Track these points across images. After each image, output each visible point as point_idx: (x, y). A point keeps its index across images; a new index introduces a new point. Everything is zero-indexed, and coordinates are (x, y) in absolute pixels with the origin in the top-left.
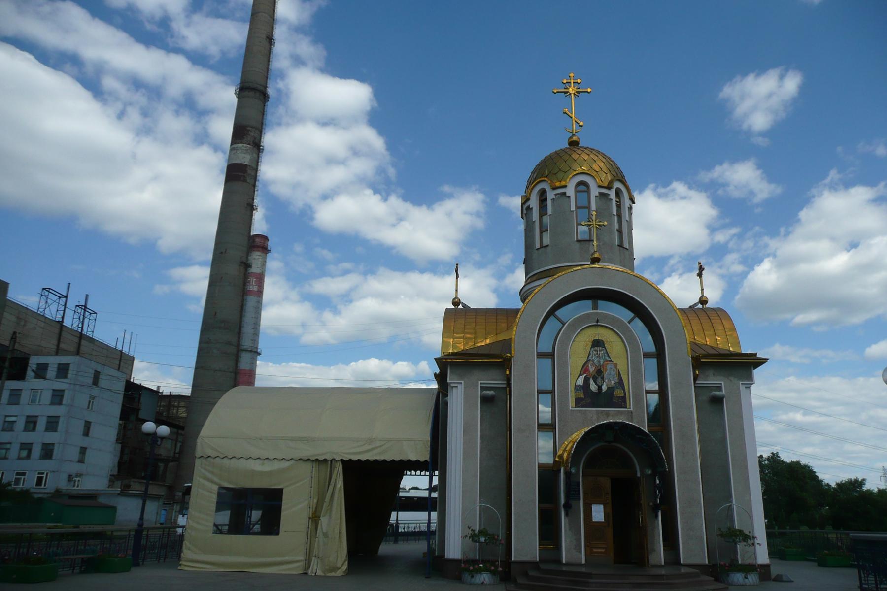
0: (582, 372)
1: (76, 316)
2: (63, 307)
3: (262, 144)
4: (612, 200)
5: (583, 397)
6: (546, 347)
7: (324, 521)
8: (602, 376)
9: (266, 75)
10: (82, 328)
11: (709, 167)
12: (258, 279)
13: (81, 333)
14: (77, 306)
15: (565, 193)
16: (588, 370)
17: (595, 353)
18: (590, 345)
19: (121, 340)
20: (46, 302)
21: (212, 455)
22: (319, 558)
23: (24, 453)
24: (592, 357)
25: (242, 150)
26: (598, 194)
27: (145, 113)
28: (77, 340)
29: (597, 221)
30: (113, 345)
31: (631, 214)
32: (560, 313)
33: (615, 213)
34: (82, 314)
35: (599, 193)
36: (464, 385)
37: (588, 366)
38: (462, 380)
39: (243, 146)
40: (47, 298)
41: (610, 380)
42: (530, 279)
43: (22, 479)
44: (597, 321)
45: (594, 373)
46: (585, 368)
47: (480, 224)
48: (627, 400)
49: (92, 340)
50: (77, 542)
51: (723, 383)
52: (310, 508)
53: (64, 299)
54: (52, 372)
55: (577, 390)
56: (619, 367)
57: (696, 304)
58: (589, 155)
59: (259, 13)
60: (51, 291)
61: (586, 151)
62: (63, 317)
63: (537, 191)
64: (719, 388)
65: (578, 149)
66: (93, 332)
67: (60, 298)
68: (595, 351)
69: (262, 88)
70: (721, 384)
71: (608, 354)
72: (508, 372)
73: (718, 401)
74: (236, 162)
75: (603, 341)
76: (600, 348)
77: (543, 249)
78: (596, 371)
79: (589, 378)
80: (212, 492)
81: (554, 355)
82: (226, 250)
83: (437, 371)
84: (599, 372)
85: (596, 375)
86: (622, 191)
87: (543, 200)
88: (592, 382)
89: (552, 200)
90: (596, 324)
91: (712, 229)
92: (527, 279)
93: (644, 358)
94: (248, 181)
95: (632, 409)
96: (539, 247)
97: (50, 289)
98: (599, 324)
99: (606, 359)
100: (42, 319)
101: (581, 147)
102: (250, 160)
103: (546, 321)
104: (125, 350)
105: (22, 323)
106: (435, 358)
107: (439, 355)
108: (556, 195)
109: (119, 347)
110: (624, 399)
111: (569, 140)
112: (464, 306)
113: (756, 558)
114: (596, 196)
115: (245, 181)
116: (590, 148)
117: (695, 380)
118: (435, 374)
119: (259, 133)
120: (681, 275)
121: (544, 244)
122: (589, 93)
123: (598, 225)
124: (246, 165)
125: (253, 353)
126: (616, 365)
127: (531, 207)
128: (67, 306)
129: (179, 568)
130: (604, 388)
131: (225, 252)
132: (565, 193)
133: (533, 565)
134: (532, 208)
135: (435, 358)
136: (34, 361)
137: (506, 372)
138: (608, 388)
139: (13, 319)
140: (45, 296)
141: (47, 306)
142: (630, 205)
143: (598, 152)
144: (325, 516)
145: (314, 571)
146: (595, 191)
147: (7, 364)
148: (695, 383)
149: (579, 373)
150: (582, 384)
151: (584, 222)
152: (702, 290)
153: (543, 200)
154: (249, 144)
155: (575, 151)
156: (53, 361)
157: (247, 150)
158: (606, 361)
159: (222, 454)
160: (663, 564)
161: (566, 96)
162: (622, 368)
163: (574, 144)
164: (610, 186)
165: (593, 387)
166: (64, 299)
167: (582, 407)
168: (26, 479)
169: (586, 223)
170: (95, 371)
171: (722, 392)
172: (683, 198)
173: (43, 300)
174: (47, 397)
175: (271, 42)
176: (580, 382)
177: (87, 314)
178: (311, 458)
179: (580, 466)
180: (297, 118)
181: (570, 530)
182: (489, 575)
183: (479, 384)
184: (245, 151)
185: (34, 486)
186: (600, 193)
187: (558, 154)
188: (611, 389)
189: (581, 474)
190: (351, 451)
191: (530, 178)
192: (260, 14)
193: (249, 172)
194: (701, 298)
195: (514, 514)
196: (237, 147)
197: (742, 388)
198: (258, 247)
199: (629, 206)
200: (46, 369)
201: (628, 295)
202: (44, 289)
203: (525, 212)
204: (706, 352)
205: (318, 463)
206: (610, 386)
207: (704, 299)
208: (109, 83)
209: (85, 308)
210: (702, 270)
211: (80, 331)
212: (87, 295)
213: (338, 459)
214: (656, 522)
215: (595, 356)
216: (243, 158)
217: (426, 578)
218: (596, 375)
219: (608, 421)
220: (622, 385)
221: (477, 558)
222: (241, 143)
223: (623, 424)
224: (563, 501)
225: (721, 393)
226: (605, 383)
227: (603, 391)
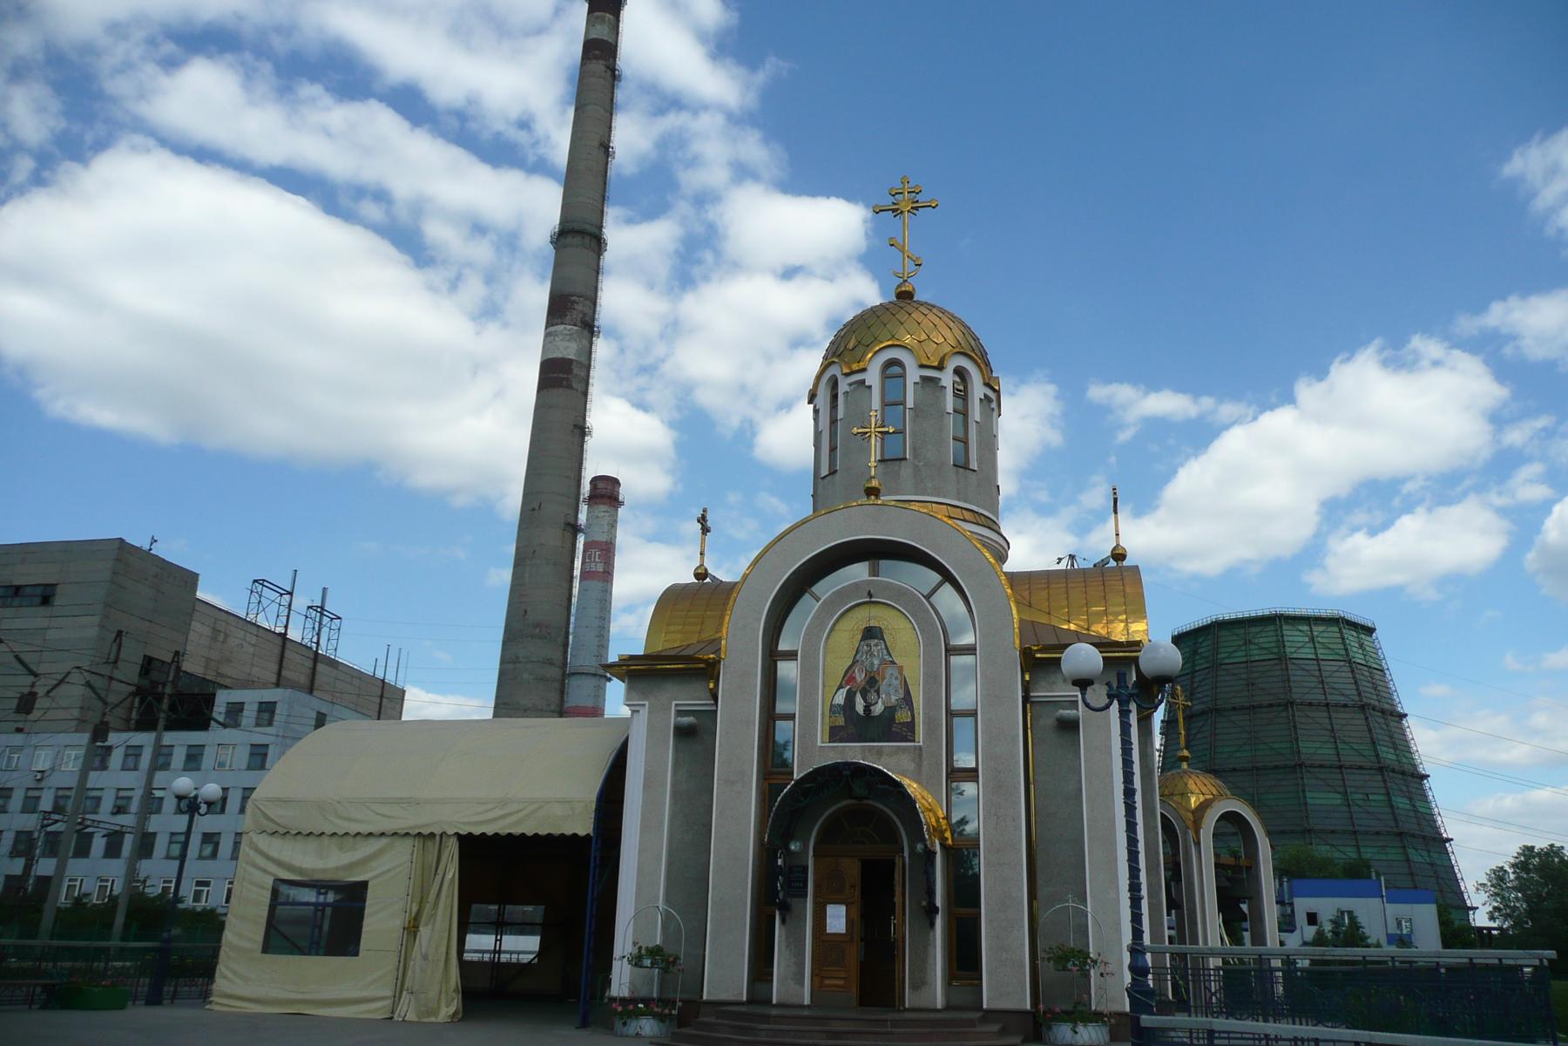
0: (843, 682)
1: (309, 624)
2: (287, 610)
3: (596, 323)
4: (945, 388)
5: (843, 724)
7: (424, 932)
8: (876, 688)
9: (601, 208)
10: (318, 643)
11: (1480, 307)
12: (604, 552)
13: (316, 653)
14: (309, 607)
15: (863, 382)
16: (855, 678)
19: (381, 663)
20: (260, 602)
21: (314, 832)
22: (412, 993)
23: (208, 850)
24: (862, 656)
25: (562, 335)
26: (918, 380)
27: (490, 279)
28: (309, 664)
30: (368, 669)
34: (318, 619)
35: (921, 377)
36: (649, 708)
37: (854, 672)
39: (565, 328)
40: (260, 596)
41: (888, 695)
43: (205, 892)
46: (848, 675)
47: (1055, 438)
49: (333, 664)
50: (136, 980)
52: (406, 912)
53: (288, 596)
54: (249, 714)
56: (906, 673)
59: (586, 105)
60: (265, 583)
61: (921, 308)
62: (286, 627)
66: (336, 649)
67: (281, 595)
69: (594, 230)
71: (888, 651)
72: (711, 686)
74: (554, 356)
76: (876, 641)
78: (868, 678)
80: (263, 888)
82: (541, 504)
86: (967, 370)
90: (868, 599)
91: (1498, 419)
94: (574, 386)
95: (921, 744)
97: (264, 580)
98: (873, 599)
99: (884, 659)
100: (254, 630)
102: (577, 351)
104: (390, 679)
105: (221, 638)
108: (850, 385)
109: (380, 675)
110: (911, 726)
111: (897, 289)
114: (915, 383)
115: (570, 387)
116: (929, 305)
119: (592, 306)
120: (1430, 510)
122: (934, 207)
124: (571, 361)
125: (598, 678)
126: (901, 669)
128: (292, 608)
129: (208, 1007)
131: (540, 507)
132: (863, 382)
136: (223, 698)
137: (708, 686)
139: (207, 631)
140: (257, 592)
141: (261, 609)
143: (943, 312)
144: (426, 925)
145: (403, 1014)
146: (913, 375)
147: (165, 706)
154: (575, 325)
155: (902, 308)
156: (251, 698)
157: (571, 335)
158: (883, 662)
159: (283, 827)
161: (895, 216)
163: (905, 296)
165: (860, 706)
166: (287, 597)
167: (841, 742)
168: (210, 892)
169: (860, 430)
170: (318, 712)
171: (1078, 710)
172: (1436, 364)
173: (255, 598)
174: (242, 756)
175: (608, 151)
176: (840, 699)
177: (326, 620)
178: (411, 832)
179: (809, 839)
180: (736, 267)
181: (787, 947)
182: (652, 1021)
183: (673, 705)
184: (568, 337)
185: (224, 904)
186: (925, 379)
187: (874, 312)
188: (890, 711)
189: (811, 853)
190: (466, 820)
192: (589, 107)
193: (576, 371)
195: (711, 921)
196: (555, 331)
198: (603, 496)
200: (242, 710)
201: (918, 548)
202: (255, 581)
205: (422, 840)
206: (889, 705)
208: (437, 231)
209: (321, 609)
211: (315, 649)
212: (325, 589)
213: (450, 832)
214: (931, 934)
216: (566, 348)
217: (576, 1028)
220: (909, 703)
221: (655, 995)
222: (562, 323)
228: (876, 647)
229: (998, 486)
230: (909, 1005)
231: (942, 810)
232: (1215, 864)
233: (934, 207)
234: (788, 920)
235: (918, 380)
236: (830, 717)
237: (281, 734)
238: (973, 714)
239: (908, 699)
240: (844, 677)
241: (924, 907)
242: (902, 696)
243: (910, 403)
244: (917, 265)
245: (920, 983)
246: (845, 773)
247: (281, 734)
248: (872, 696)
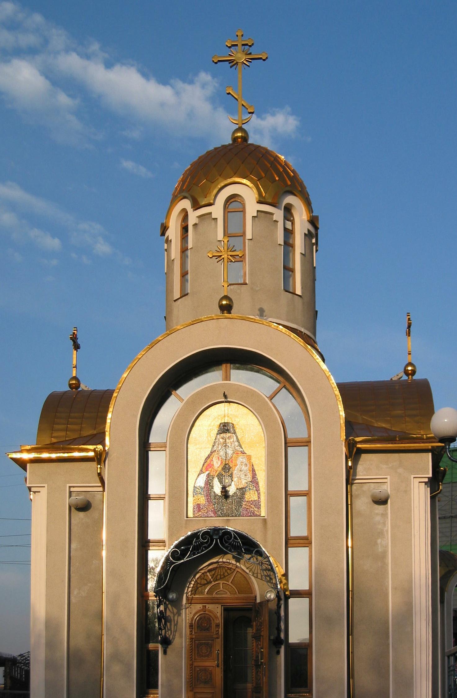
16: (213, 465)
18: (216, 431)
45: (220, 469)
51: (388, 477)
56: (253, 460)
84: (227, 468)
89: (193, 225)
108: (199, 217)
122: (264, 60)
126: (249, 458)
130: (232, 490)
134: (171, 241)
158: (235, 452)
161: (231, 67)
188: (242, 491)
226: (233, 482)
228: (231, 441)
229: (317, 311)
231: (282, 568)
232: (454, 617)
233: (264, 60)
237: (80, 432)
238: (306, 494)
239: (254, 481)
240: (204, 465)
242: (250, 479)
243: (249, 235)
244: (250, 113)
247: (80, 432)
248: (227, 481)
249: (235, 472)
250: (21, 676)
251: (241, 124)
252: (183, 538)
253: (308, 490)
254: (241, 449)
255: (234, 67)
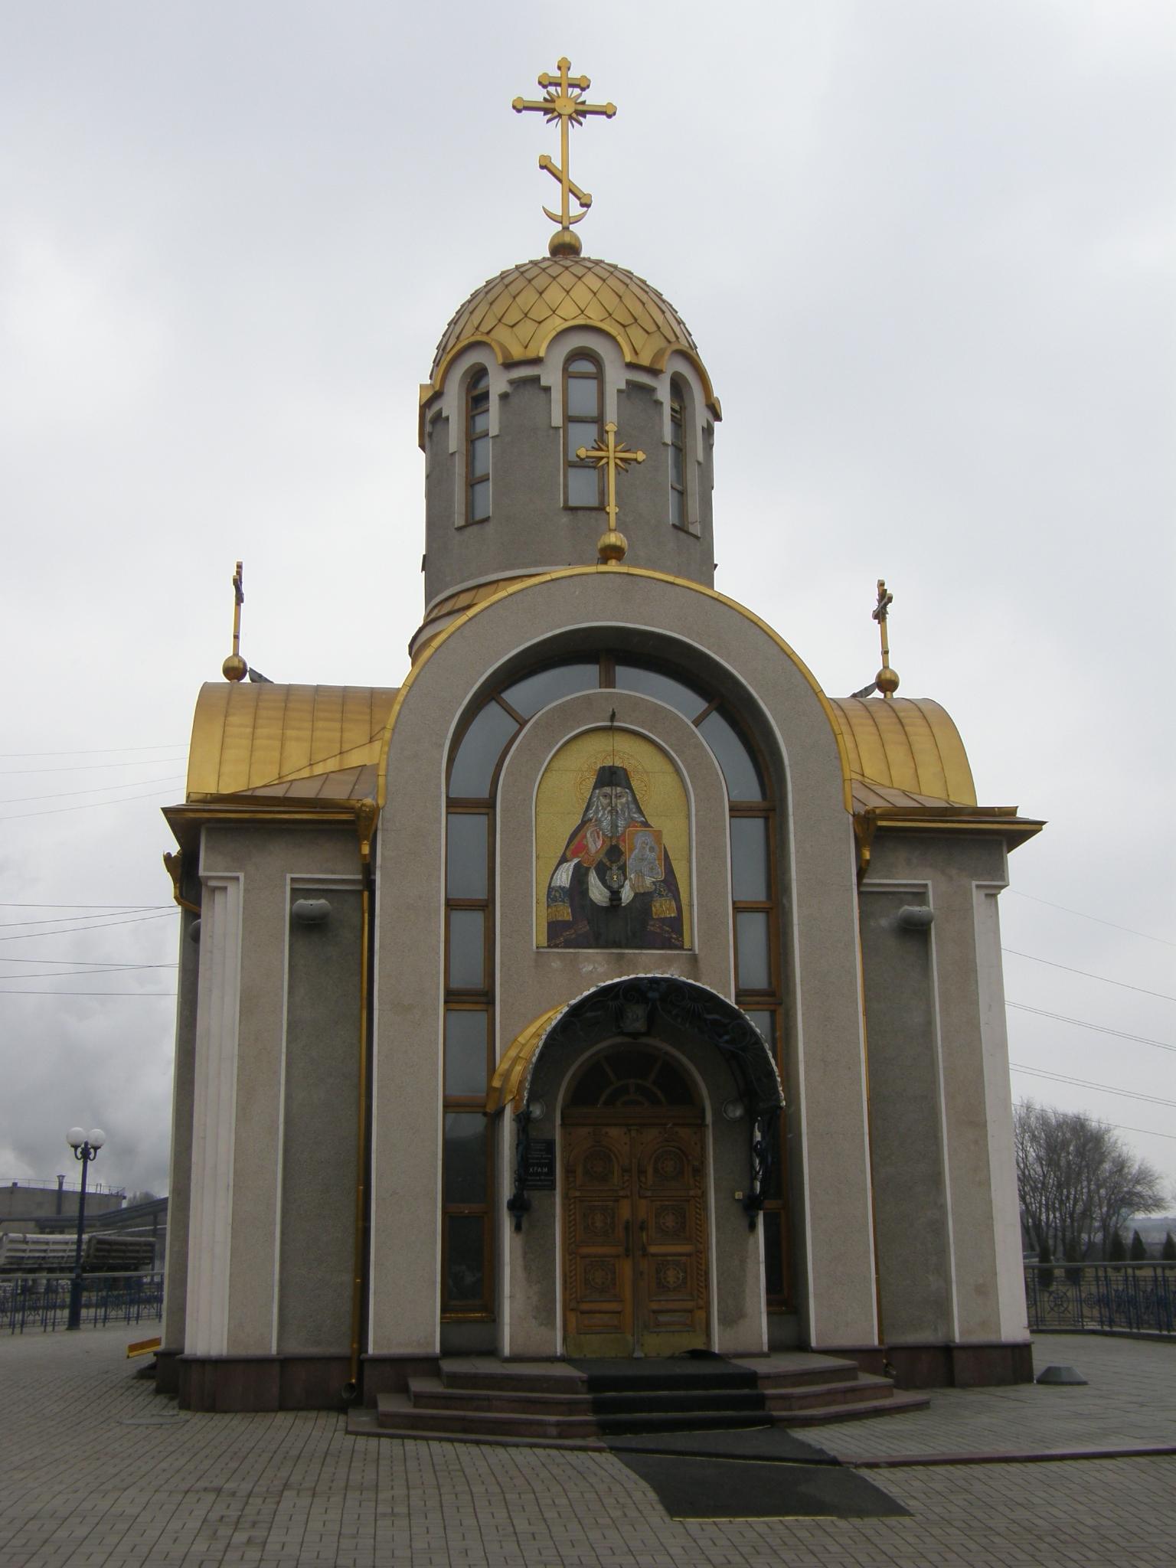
0: (568, 854)
6: (473, 787)
15: (536, 379)
16: (587, 846)
17: (605, 801)
24: (597, 812)
26: (623, 386)
29: (619, 448)
31: (709, 447)
32: (515, 695)
33: (669, 440)
38: (240, 869)
41: (640, 874)
42: (436, 611)
44: (613, 717)
46: (576, 841)
48: (686, 927)
51: (929, 882)
55: (555, 900)
56: (667, 841)
57: (867, 691)
58: (604, 280)
63: (461, 374)
64: (920, 896)
65: (577, 262)
68: (605, 796)
70: (926, 886)
73: (916, 931)
75: (625, 770)
76: (619, 789)
77: (475, 529)
78: (605, 848)
79: (588, 869)
81: (493, 806)
83: (174, 848)
84: (614, 852)
85: (605, 860)
87: (477, 401)
88: (593, 879)
90: (609, 724)
92: (428, 611)
93: (731, 817)
96: (462, 523)
98: (616, 724)
101: (584, 259)
103: (476, 715)
106: (163, 809)
107: (179, 799)
108: (511, 382)
112: (257, 678)
113: (999, 1331)
117: (861, 874)
118: (168, 858)
121: (479, 516)
123: (621, 459)
126: (658, 835)
127: (444, 415)
130: (627, 895)
132: (536, 379)
133: (427, 1365)
134: (447, 418)
135: (163, 809)
138: (636, 895)
142: (708, 423)
146: (616, 378)
148: (859, 884)
149: (560, 854)
150: (568, 886)
151: (583, 450)
152: (885, 653)
153: (477, 401)
158: (631, 822)
160: (765, 1348)
161: (548, 121)
162: (672, 842)
164: (658, 367)
165: (598, 893)
171: (929, 906)
176: (564, 877)
183: (288, 881)
188: (643, 899)
189: (558, 1121)
191: (444, 336)
194: (879, 676)
197: (978, 897)
199: (706, 426)
203: (428, 428)
204: (892, 804)
207: (888, 676)
210: (886, 600)
215: (604, 809)
218: (605, 860)
219: (632, 976)
220: (673, 888)
223: (673, 986)
224: (506, 1189)
225: (924, 908)
226: (627, 882)
227: (623, 905)
230: (719, 1350)
234: (525, 1225)
235: (623, 386)
236: (548, 906)
239: (670, 882)
241: (738, 1200)
242: (661, 877)
245: (733, 1317)
246: (651, 995)
248: (615, 877)
249: (631, 862)
250: (1088, 1277)
251: (568, 223)
252: (593, 990)
253: (487, 898)
254: (643, 819)
255: (553, 121)
